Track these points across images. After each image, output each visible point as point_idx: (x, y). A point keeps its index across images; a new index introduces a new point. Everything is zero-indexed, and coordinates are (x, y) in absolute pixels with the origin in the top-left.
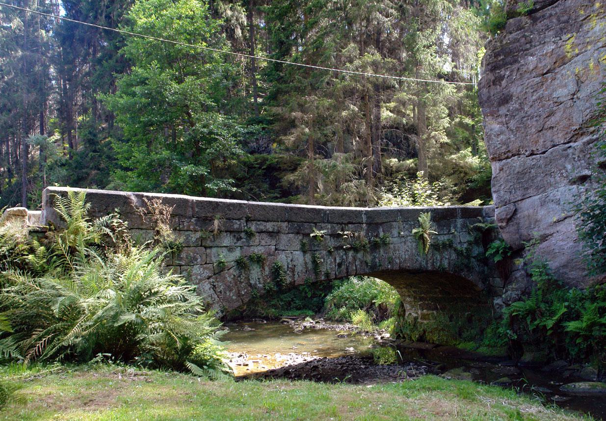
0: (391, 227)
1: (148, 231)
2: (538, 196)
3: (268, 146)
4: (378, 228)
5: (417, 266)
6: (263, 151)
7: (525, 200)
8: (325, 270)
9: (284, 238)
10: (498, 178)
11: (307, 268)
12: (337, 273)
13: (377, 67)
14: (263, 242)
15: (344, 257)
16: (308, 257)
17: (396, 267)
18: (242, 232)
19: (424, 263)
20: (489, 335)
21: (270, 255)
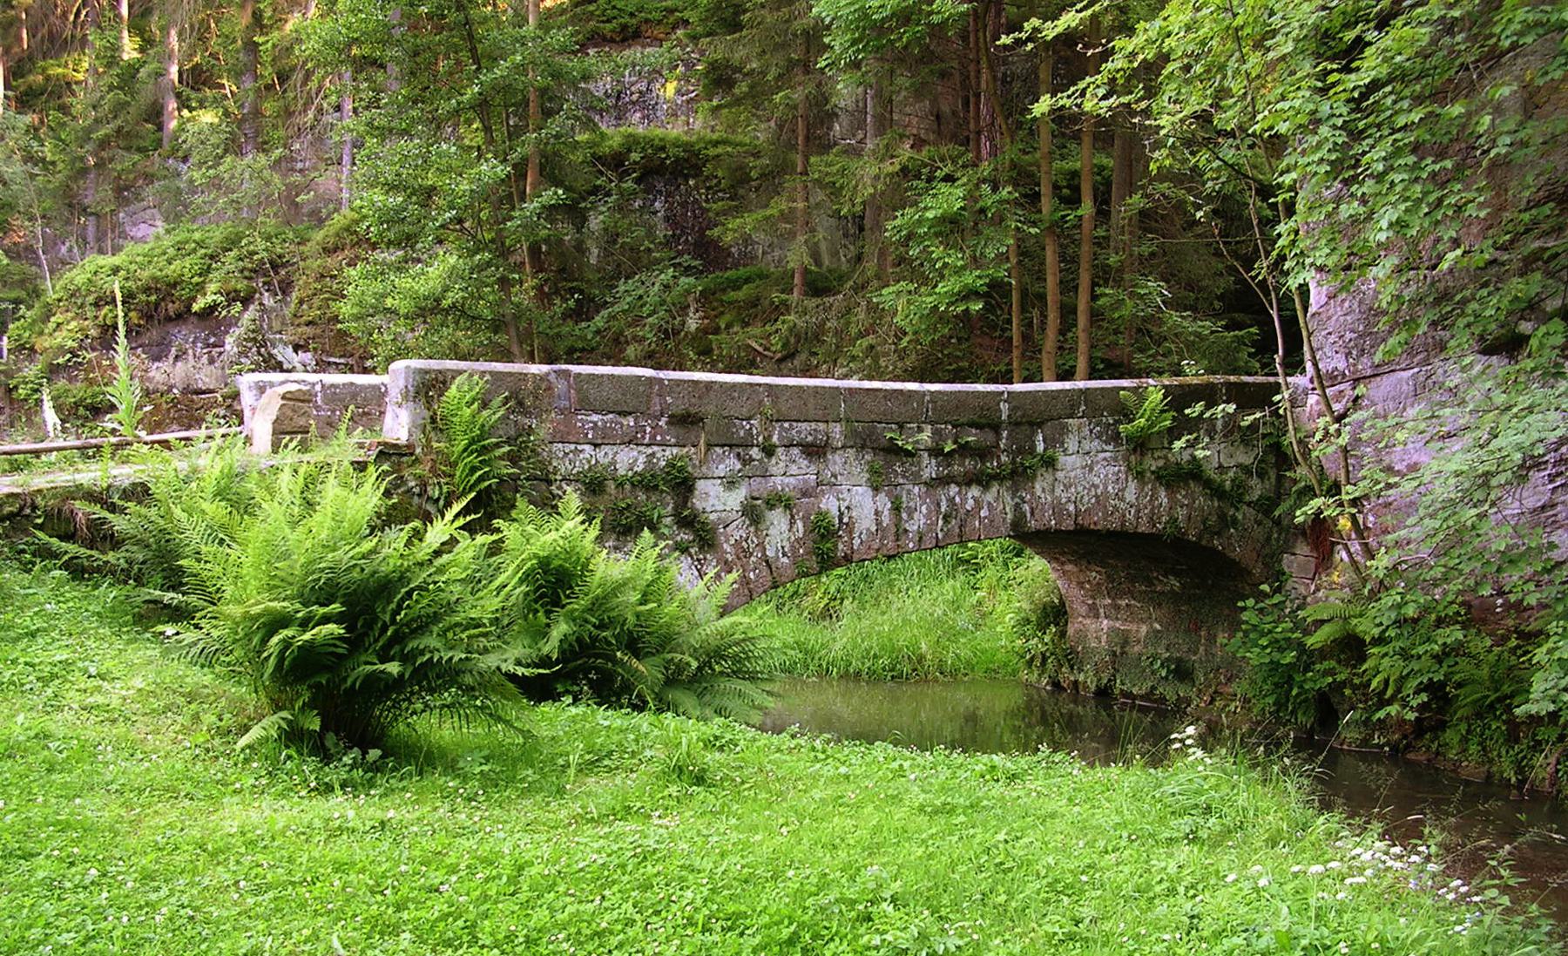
0: (1064, 430)
1: (579, 447)
2: (1412, 371)
3: (649, 90)
4: (1034, 433)
5: (1115, 525)
6: (634, 103)
7: (1378, 379)
8: (916, 528)
9: (836, 461)
10: (1324, 316)
11: (879, 523)
12: (940, 536)
13: (1099, 244)
14: (793, 469)
15: (957, 499)
16: (884, 503)
17: (1068, 525)
18: (752, 446)
19: (1130, 517)
20: (164, 910)
21: (805, 494)
